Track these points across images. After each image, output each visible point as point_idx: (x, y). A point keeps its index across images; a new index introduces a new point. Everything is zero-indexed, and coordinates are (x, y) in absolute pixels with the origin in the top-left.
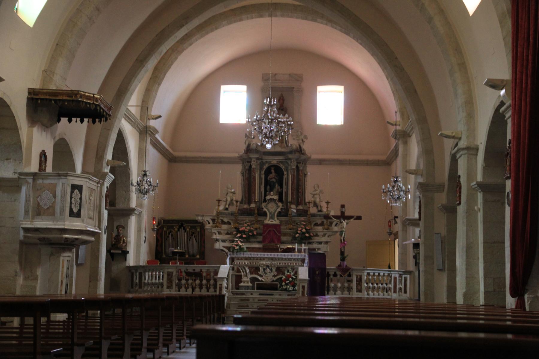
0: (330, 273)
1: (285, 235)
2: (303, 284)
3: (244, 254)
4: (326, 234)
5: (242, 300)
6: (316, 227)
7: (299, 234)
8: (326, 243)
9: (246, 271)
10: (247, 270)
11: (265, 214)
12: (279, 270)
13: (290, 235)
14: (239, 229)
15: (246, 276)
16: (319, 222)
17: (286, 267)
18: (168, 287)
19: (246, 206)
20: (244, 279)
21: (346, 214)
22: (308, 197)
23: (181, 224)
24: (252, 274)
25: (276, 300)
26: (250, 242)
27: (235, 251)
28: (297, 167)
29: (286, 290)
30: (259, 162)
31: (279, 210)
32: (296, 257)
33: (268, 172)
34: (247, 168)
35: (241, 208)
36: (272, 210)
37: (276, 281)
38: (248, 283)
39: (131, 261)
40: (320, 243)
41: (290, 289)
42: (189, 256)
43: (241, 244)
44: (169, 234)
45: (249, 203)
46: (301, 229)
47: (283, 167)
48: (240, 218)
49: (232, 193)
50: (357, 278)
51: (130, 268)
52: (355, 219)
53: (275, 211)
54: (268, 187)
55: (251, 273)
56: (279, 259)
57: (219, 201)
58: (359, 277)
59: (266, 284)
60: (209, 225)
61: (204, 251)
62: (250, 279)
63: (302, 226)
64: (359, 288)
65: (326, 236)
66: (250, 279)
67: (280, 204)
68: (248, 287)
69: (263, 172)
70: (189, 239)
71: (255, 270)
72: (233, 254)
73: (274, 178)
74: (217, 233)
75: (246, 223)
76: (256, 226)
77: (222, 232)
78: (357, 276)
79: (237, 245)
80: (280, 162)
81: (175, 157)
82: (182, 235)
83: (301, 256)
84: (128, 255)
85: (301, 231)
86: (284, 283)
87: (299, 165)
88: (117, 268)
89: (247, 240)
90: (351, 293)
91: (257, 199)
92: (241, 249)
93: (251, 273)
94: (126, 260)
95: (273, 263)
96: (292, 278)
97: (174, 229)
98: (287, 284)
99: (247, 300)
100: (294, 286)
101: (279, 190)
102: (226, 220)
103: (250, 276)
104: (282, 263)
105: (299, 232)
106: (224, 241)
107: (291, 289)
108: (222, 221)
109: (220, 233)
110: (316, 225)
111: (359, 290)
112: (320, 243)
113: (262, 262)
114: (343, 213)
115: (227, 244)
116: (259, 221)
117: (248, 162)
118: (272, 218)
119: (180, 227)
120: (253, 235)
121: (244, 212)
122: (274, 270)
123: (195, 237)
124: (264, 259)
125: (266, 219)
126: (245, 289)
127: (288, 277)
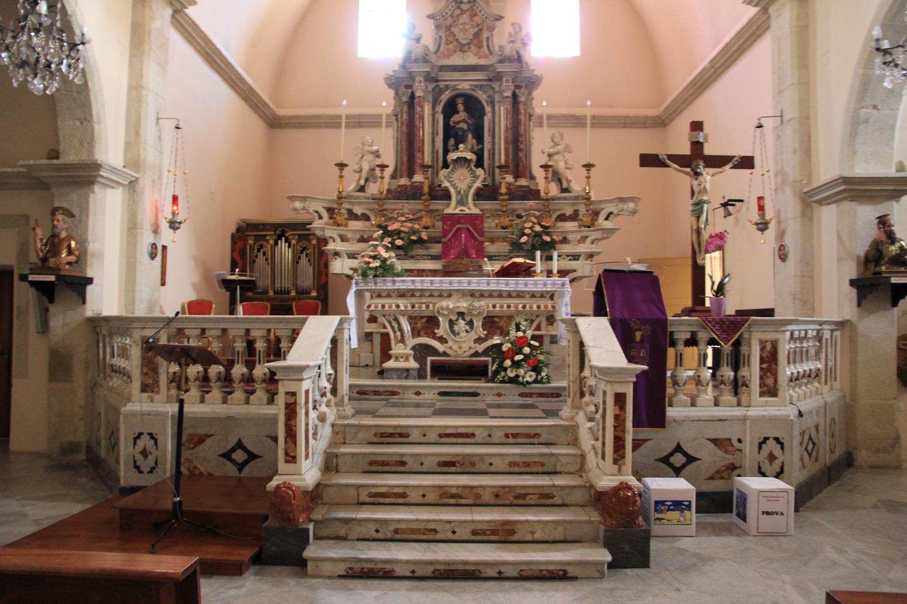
0: (676, 336)
1: (492, 240)
2: (620, 389)
3: (394, 282)
4: (587, 237)
5: (382, 435)
6: (559, 224)
7: (528, 235)
8: (590, 256)
9: (401, 329)
10: (406, 326)
11: (446, 196)
12: (492, 324)
13: (504, 239)
14: (387, 226)
15: (402, 341)
16: (569, 211)
17: (510, 318)
18: (144, 388)
19: (404, 181)
20: (397, 349)
21: (708, 151)
22: (537, 160)
23: (281, 231)
24: (419, 335)
25: (536, 497)
26: (412, 257)
27: (371, 273)
28: (515, 96)
29: (514, 380)
30: (431, 86)
31: (478, 184)
32: (540, 288)
33: (450, 109)
34: (405, 99)
35: (393, 187)
36: (462, 186)
37: (485, 353)
38: (407, 359)
39: (105, 298)
40: (575, 257)
41: (528, 379)
42: (297, 293)
43: (385, 255)
44: (259, 250)
45: (410, 175)
46: (531, 224)
47: (482, 96)
48: (391, 205)
49: (372, 153)
50: (762, 349)
51: (99, 327)
52: (734, 167)
53: (470, 187)
54: (452, 141)
55: (416, 333)
56: (491, 294)
57: (342, 166)
58: (769, 347)
59: (455, 363)
60: (320, 221)
61: (327, 283)
62: (413, 348)
63: (533, 219)
64: (770, 381)
65: (588, 240)
66: (413, 348)
67: (480, 171)
68: (407, 370)
69: (439, 108)
70: (296, 261)
71: (427, 324)
72: (366, 283)
73: (465, 122)
74: (338, 239)
75: (402, 216)
76: (426, 221)
77: (349, 235)
78: (763, 343)
79: (374, 258)
80: (476, 86)
81: (279, 118)
82: (285, 251)
83: (554, 284)
84: (89, 288)
85: (531, 228)
86: (508, 363)
87: (517, 91)
88: (63, 320)
89: (404, 252)
90: (744, 399)
91: (427, 160)
92: (386, 269)
93: (416, 333)
94: (84, 302)
95: (476, 304)
96: (530, 346)
97: (268, 241)
98: (516, 365)
99: (401, 435)
100: (536, 369)
101: (476, 148)
102: (358, 210)
103: (412, 342)
104: (500, 306)
105: (527, 231)
106: (352, 256)
107: (530, 377)
108: (350, 212)
109: (344, 239)
110: (562, 218)
111: (770, 391)
112: (575, 257)
113: (444, 303)
114: (697, 146)
115: (354, 263)
116: (432, 211)
117: (407, 87)
118: (461, 202)
119: (279, 238)
120: (420, 241)
121: (411, 193)
122: (478, 323)
123: (307, 255)
124: (449, 294)
125: (448, 205)
126: (399, 378)
127: (519, 344)
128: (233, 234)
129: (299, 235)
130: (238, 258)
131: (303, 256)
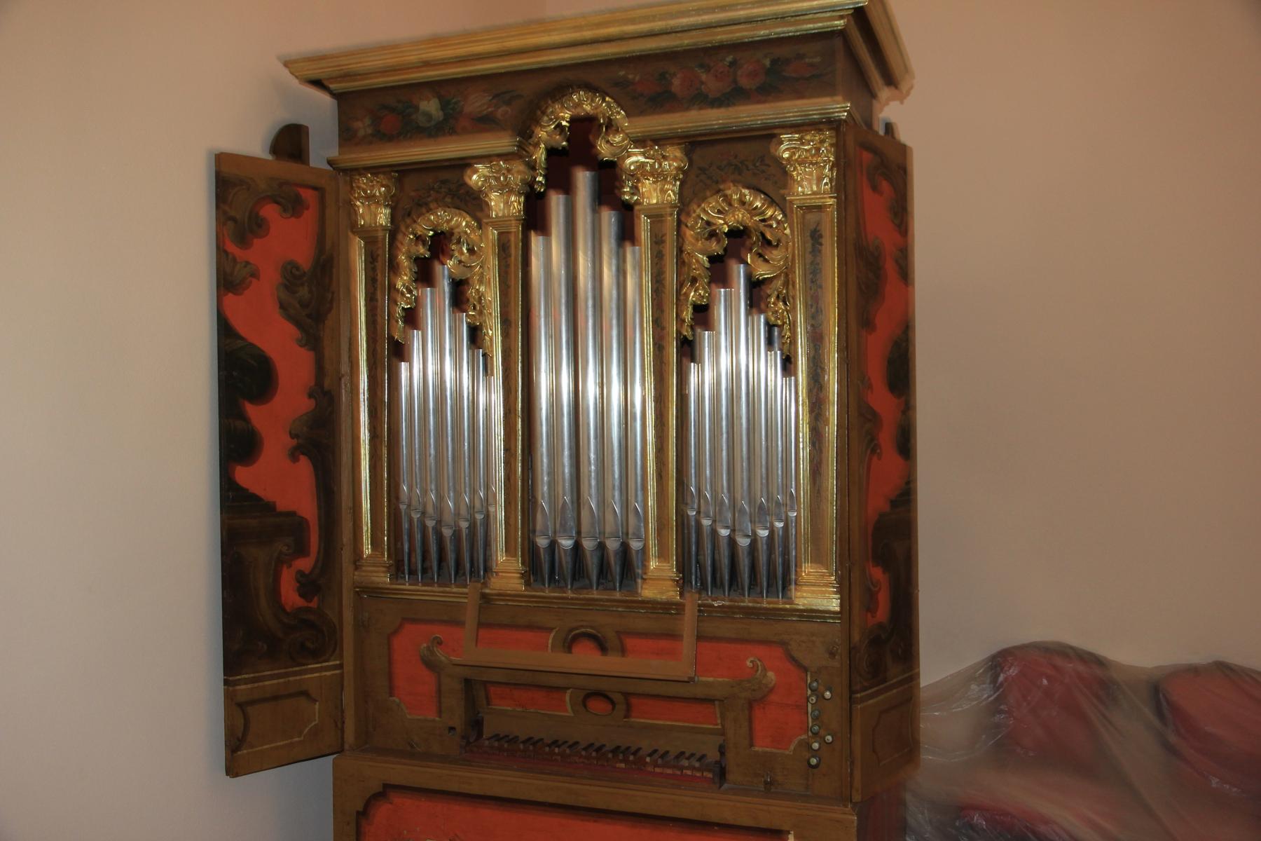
129: (692, 143)
130: (276, 338)
131: (730, 304)
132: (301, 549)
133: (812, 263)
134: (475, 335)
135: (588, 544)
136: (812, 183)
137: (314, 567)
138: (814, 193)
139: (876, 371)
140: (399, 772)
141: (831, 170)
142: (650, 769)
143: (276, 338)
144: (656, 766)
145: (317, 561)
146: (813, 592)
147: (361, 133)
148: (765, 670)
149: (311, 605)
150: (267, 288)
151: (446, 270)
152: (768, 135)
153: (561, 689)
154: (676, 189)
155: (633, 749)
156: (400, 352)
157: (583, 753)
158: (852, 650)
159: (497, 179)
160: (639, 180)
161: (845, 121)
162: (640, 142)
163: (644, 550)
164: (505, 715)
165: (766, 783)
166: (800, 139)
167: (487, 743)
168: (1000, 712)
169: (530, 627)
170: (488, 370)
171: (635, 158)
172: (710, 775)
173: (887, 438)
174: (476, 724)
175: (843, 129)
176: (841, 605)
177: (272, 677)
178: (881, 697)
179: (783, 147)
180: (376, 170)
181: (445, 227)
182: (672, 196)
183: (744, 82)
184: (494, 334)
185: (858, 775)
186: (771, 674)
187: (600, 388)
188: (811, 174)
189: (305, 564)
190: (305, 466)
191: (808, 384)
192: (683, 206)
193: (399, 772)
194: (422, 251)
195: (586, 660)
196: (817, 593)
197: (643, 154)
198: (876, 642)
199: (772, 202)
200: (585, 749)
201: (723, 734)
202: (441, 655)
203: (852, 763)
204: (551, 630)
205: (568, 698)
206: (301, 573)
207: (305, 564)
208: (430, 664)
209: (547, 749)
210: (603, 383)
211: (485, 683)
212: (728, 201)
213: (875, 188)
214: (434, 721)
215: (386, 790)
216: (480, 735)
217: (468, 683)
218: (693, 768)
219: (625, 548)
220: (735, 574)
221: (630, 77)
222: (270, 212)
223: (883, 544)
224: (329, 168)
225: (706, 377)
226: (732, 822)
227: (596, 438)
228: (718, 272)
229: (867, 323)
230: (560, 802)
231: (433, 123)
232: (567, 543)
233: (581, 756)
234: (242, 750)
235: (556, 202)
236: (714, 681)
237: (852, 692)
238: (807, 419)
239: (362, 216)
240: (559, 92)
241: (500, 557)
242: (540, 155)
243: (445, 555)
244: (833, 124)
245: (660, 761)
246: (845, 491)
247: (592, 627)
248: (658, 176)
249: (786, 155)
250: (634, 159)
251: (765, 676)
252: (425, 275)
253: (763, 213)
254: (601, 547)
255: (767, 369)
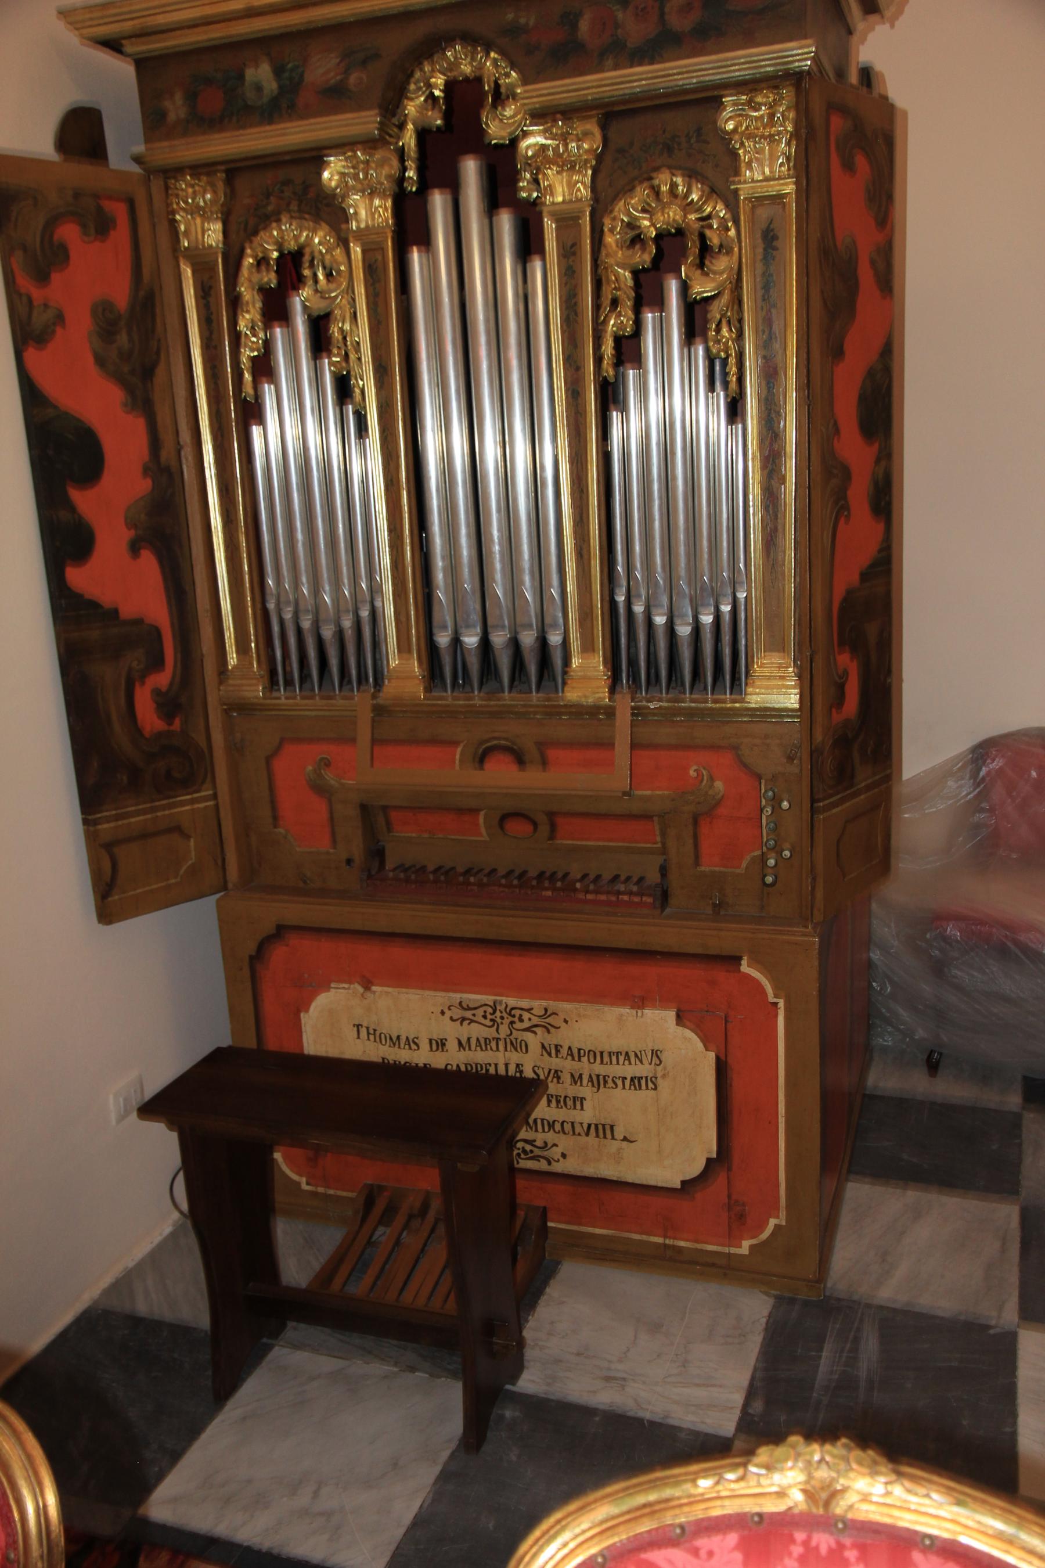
128: (863, 44)
129: (611, 114)
130: (96, 401)
131: (663, 331)
132: (157, 662)
133: (764, 274)
134: (344, 389)
135: (499, 639)
136: (767, 168)
137: (171, 684)
138: (767, 179)
139: (847, 410)
140: (294, 911)
141: (788, 144)
142: (581, 896)
143: (96, 401)
144: (587, 892)
145: (173, 677)
146: (767, 687)
147: (172, 117)
148: (712, 779)
149: (172, 728)
150: (78, 333)
151: (300, 301)
152: (709, 98)
153: (474, 811)
154: (588, 180)
155: (560, 875)
156: (252, 412)
157: (503, 881)
158: (815, 753)
159: (356, 177)
160: (538, 169)
161: (808, 73)
162: (540, 115)
163: (565, 643)
164: (409, 842)
165: (714, 905)
166: (749, 102)
167: (391, 874)
168: (982, 810)
169: (434, 741)
170: (362, 429)
171: (534, 140)
172: (650, 900)
173: (859, 494)
174: (378, 854)
175: (806, 84)
176: (801, 701)
177: (138, 813)
178: (848, 804)
179: (725, 114)
180: (200, 169)
181: (292, 246)
182: (584, 191)
183: (677, 22)
184: (367, 382)
185: (819, 894)
186: (719, 785)
187: (501, 447)
188: (763, 150)
189: (162, 679)
190: (148, 560)
191: (760, 433)
192: (601, 205)
193: (294, 911)
194: (271, 279)
195: (501, 777)
196: (776, 688)
197: (545, 131)
198: (843, 741)
199: (713, 192)
200: (504, 877)
201: (664, 851)
202: (330, 778)
203: (814, 879)
204: (455, 743)
205: (481, 820)
206: (157, 692)
207: (162, 679)
208: (320, 789)
209: (461, 879)
210: (505, 441)
211: (385, 808)
212: (656, 192)
213: (849, 166)
214: (328, 853)
215: (281, 931)
216: (382, 863)
217: (365, 809)
218: (631, 893)
219: (543, 642)
220: (676, 668)
221: (522, 21)
222: (69, 233)
223: (856, 628)
224: (136, 169)
225: (633, 428)
226: (676, 950)
227: (499, 511)
228: (647, 293)
229: (836, 352)
230: (479, 936)
231: (265, 100)
232: (471, 640)
233: (500, 885)
234: (113, 894)
235: (438, 202)
236: (655, 793)
237: (813, 801)
238: (758, 477)
239: (187, 233)
240: (430, 48)
241: (394, 661)
242: (409, 139)
243: (325, 660)
244: (796, 78)
245: (592, 887)
246: (806, 564)
247: (506, 739)
248: (568, 165)
249: (730, 126)
250: (531, 140)
251: (711, 786)
252: (276, 310)
253: (700, 210)
254: (515, 643)
255: (708, 416)
